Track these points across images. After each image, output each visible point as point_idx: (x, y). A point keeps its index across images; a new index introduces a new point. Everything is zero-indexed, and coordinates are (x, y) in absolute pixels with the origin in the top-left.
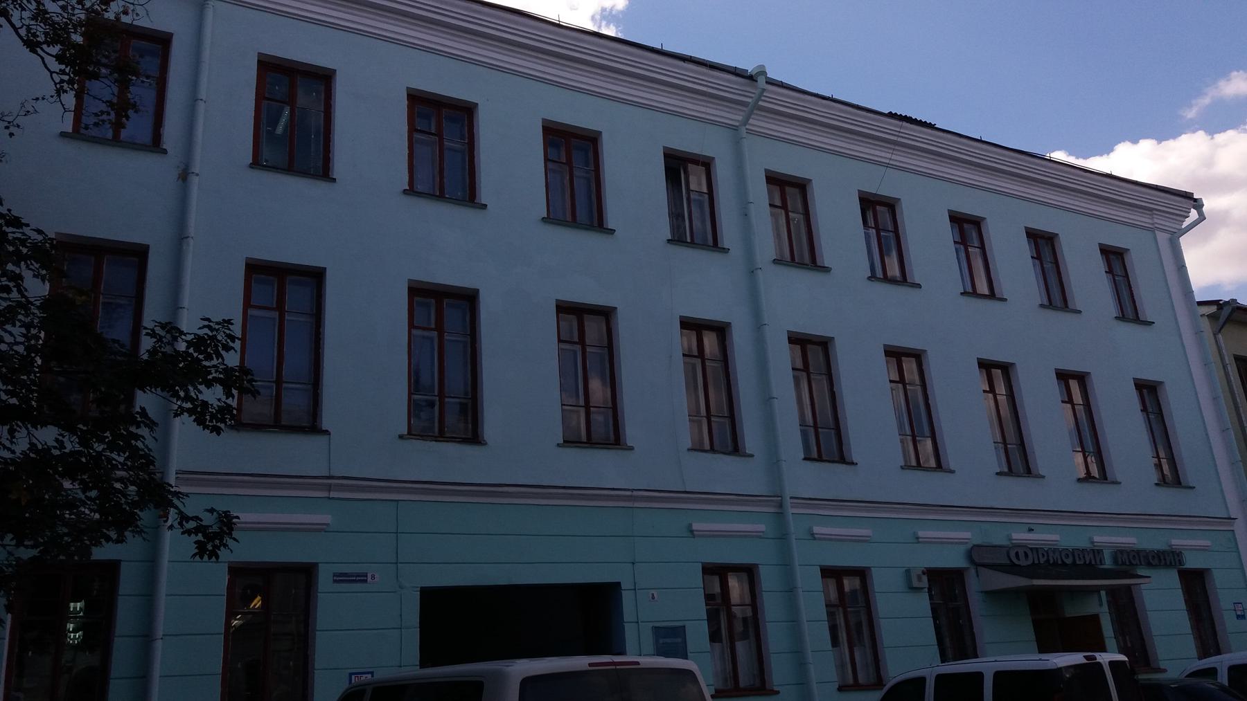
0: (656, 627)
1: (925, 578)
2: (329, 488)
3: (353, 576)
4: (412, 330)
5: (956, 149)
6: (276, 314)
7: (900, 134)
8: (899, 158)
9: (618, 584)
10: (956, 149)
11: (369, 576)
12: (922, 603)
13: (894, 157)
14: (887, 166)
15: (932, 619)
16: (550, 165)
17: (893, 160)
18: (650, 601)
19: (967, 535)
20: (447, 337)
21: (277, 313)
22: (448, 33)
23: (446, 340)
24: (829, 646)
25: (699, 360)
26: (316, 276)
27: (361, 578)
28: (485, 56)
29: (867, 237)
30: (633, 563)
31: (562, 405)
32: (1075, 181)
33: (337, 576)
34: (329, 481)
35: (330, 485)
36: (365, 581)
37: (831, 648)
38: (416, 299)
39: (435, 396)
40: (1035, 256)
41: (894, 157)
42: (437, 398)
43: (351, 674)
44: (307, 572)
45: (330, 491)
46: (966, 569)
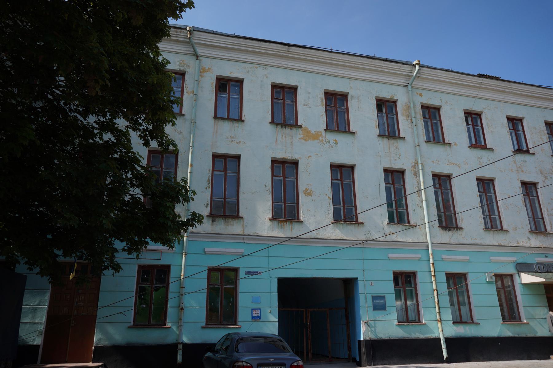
0: (372, 296)
1: (494, 278)
2: (243, 239)
3: (252, 272)
4: (273, 177)
5: (526, 91)
6: (223, 173)
7: (383, 67)
9: (357, 278)
10: (526, 91)
11: (258, 273)
12: (493, 289)
13: (479, 94)
14: (476, 98)
15: (497, 295)
16: (328, 108)
17: (479, 95)
18: (370, 286)
20: (286, 179)
21: (224, 173)
22: (376, 74)
23: (287, 180)
24: (449, 305)
25: (393, 185)
26: (238, 158)
27: (255, 273)
28: (228, 56)
29: (468, 129)
30: (364, 270)
31: (333, 206)
32: (295, 53)
33: (247, 272)
34: (243, 237)
35: (243, 238)
36: (257, 274)
37: (450, 306)
38: (275, 165)
39: (282, 203)
40: (550, 133)
41: (479, 94)
42: (283, 204)
43: (252, 309)
44: (236, 270)
45: (243, 240)
46: (514, 274)
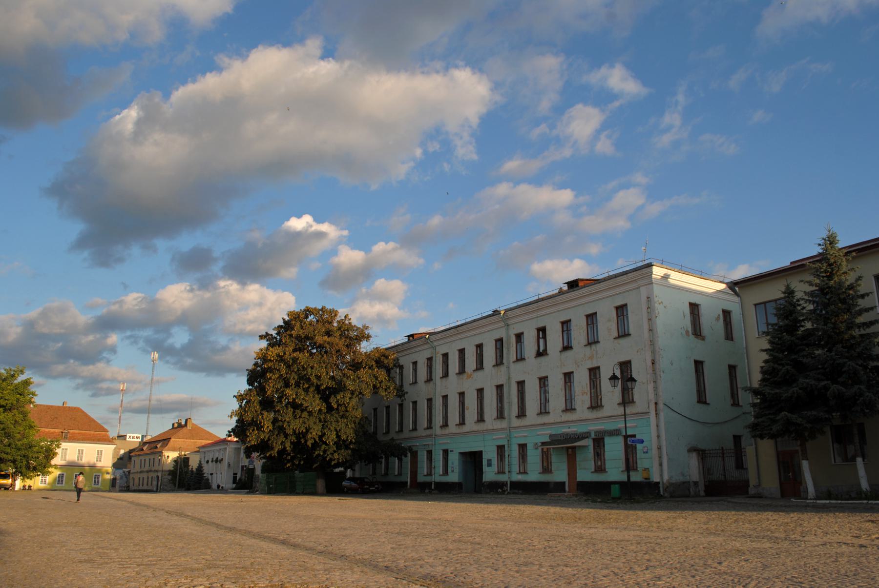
8: (539, 313)
14: (537, 317)
19: (550, 432)
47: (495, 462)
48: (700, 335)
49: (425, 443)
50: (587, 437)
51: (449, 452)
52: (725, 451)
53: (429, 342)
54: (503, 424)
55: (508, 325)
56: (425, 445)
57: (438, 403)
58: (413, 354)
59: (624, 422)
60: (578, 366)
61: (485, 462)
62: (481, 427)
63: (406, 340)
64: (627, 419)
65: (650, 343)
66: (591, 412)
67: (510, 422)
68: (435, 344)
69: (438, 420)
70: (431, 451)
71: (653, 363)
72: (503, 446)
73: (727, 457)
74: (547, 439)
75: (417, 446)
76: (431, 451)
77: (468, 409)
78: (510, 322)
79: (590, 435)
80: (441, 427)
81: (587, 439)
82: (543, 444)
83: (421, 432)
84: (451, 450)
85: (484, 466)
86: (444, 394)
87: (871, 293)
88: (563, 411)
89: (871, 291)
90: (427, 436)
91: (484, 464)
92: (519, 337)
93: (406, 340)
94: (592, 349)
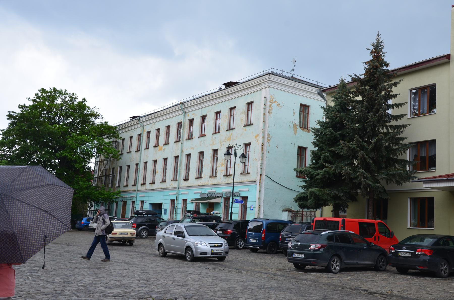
19: (200, 191)
47: (168, 211)
48: (307, 129)
49: (131, 196)
50: (221, 197)
51: (144, 203)
52: (304, 213)
53: (140, 122)
54: (175, 184)
55: (185, 113)
56: (131, 197)
57: (142, 166)
58: (131, 131)
59: (232, 187)
60: (221, 145)
61: (163, 211)
62: (164, 186)
63: (129, 120)
64: (234, 186)
65: (262, 131)
66: (225, 178)
67: (179, 184)
68: (144, 124)
69: (140, 180)
70: (134, 201)
71: (262, 146)
72: (174, 200)
73: (305, 217)
74: (198, 197)
75: (127, 197)
76: (134, 201)
77: (157, 173)
78: (186, 110)
79: (223, 195)
80: (142, 185)
81: (221, 198)
82: (196, 200)
83: (130, 188)
84: (145, 201)
85: (162, 214)
86: (145, 161)
87: (406, 103)
88: (210, 177)
89: (406, 102)
90: (133, 191)
91: (162, 212)
92: (191, 121)
93: (129, 120)
94: (231, 133)
